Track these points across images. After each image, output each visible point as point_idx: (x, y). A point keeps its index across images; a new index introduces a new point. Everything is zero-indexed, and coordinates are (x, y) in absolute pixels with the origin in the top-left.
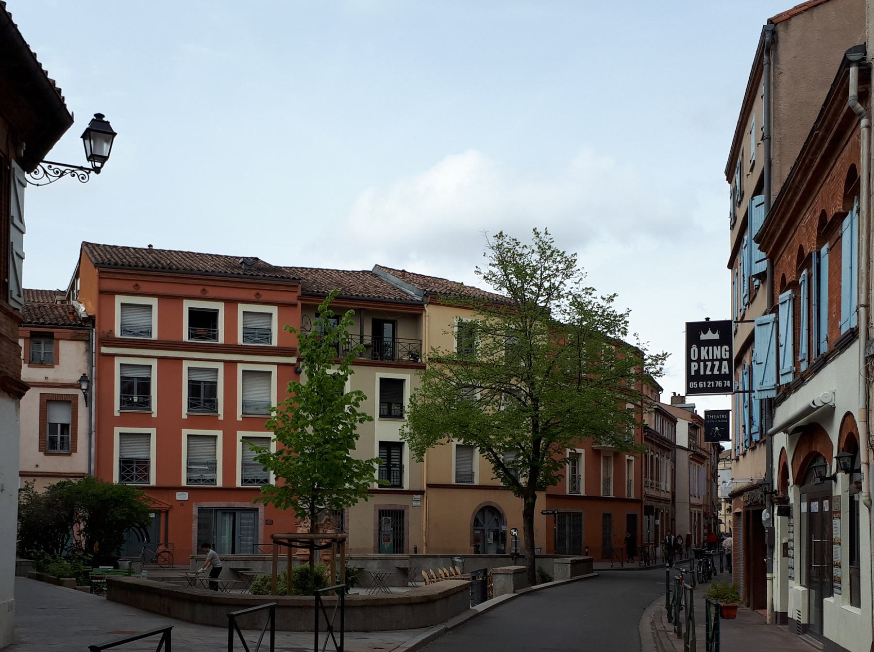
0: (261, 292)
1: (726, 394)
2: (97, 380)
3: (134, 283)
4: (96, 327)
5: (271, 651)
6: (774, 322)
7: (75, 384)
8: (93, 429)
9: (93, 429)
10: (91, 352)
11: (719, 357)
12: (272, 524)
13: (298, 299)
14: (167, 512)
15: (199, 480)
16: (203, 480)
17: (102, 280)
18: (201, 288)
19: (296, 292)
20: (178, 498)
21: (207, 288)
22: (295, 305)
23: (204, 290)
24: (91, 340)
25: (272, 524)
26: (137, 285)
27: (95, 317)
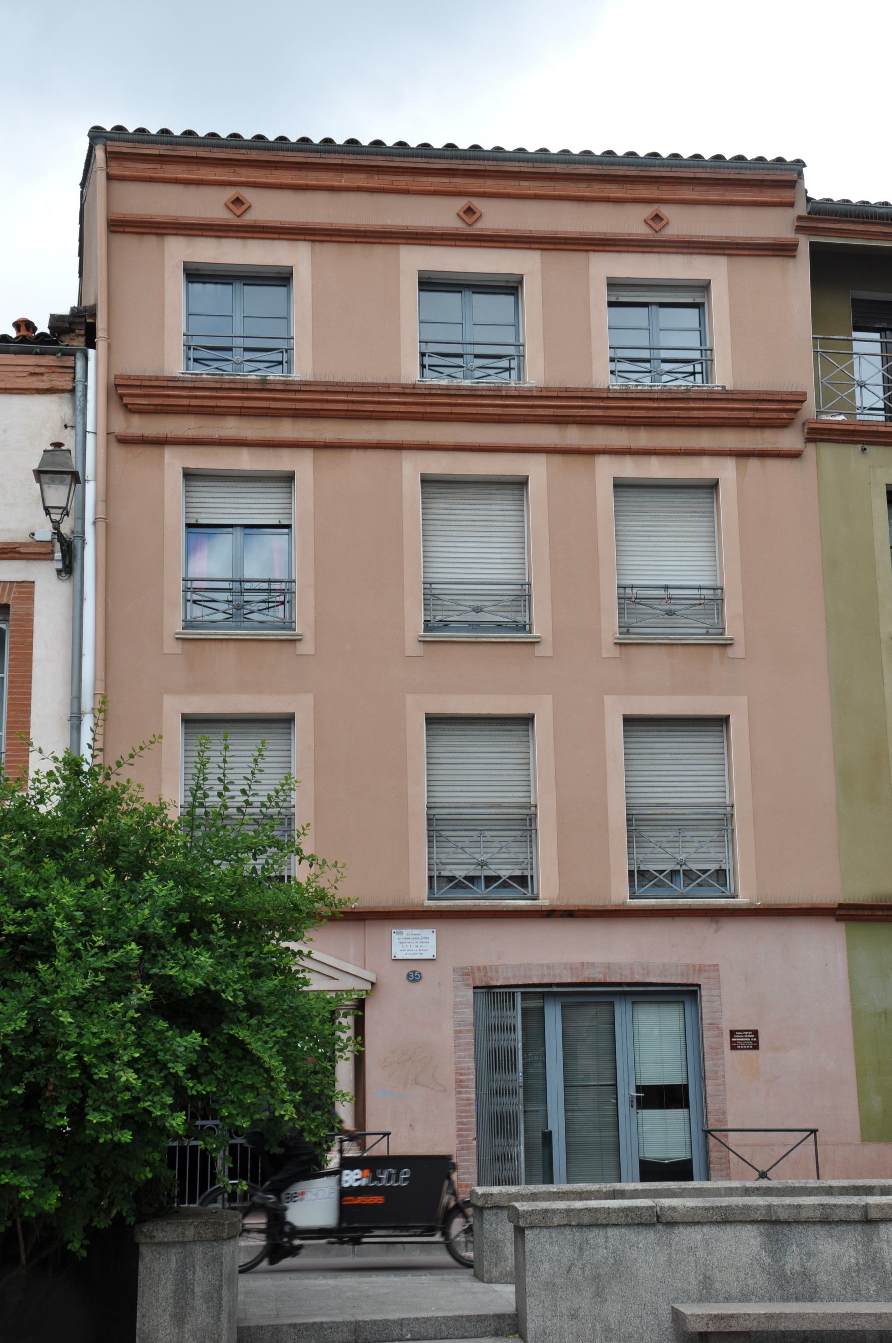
0: (666, 211)
1: (204, 283)
2: (101, 525)
3: (230, 193)
4: (101, 344)
5: (889, 1225)
6: (85, 480)
7: (22, 544)
8: (87, 702)
9: (87, 702)
10: (79, 428)
11: (697, 375)
12: (756, 1047)
13: (799, 229)
14: (361, 1004)
15: (472, 879)
16: (489, 880)
17: (117, 186)
18: (461, 203)
19: (791, 205)
20: (399, 952)
21: (478, 204)
22: (785, 250)
23: (470, 210)
24: (79, 388)
25: (756, 1047)
26: (238, 201)
27: (94, 315)
